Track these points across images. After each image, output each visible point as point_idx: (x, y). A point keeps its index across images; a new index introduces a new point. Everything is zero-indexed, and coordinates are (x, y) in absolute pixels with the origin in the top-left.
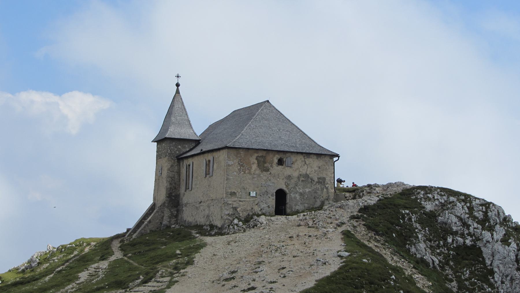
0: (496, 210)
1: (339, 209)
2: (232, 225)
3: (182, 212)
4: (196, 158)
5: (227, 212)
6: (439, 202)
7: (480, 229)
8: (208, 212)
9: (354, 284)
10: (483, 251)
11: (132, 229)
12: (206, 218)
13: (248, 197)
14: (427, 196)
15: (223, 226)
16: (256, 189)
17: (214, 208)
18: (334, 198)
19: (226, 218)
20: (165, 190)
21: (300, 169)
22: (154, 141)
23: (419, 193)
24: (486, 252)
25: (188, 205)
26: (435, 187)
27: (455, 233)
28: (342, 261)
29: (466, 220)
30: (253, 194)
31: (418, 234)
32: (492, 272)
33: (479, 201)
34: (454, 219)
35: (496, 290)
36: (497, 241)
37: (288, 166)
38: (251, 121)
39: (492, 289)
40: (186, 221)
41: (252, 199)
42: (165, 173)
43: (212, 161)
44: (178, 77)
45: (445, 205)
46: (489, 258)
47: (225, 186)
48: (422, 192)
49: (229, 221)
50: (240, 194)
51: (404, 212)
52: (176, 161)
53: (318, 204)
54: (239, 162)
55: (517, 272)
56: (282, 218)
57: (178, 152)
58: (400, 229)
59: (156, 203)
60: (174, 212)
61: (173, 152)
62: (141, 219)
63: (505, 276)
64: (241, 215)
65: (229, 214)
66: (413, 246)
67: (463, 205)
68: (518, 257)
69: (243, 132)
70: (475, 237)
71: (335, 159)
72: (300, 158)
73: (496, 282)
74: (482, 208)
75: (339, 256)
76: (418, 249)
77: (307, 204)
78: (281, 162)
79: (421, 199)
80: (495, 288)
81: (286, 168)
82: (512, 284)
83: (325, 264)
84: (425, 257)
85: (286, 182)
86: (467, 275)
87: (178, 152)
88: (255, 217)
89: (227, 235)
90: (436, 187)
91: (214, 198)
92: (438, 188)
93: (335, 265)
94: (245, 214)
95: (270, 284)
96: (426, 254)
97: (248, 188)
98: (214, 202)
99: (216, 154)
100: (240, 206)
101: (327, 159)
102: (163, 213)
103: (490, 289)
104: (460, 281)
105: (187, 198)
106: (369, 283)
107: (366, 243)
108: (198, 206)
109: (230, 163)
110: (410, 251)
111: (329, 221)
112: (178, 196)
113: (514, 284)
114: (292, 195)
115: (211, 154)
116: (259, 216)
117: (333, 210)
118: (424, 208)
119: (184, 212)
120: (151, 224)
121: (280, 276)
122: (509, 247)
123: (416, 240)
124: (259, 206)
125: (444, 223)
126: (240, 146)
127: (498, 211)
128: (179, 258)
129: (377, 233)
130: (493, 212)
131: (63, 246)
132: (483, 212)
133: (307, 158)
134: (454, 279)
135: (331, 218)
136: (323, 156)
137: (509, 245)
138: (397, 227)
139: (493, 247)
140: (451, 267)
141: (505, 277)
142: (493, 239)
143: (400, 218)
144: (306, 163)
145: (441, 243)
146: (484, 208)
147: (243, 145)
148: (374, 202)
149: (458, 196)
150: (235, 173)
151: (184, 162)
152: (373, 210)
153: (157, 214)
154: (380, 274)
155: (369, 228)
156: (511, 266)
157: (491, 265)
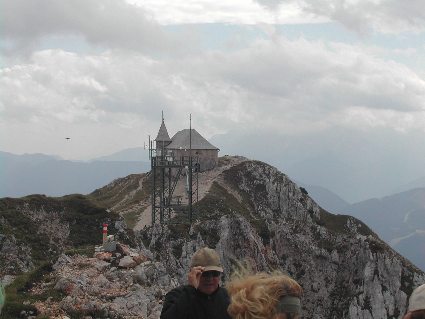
0: (273, 171)
24: (267, 186)
34: (257, 174)
73: (269, 197)
140: (253, 192)
142: (269, 182)
145: (252, 183)
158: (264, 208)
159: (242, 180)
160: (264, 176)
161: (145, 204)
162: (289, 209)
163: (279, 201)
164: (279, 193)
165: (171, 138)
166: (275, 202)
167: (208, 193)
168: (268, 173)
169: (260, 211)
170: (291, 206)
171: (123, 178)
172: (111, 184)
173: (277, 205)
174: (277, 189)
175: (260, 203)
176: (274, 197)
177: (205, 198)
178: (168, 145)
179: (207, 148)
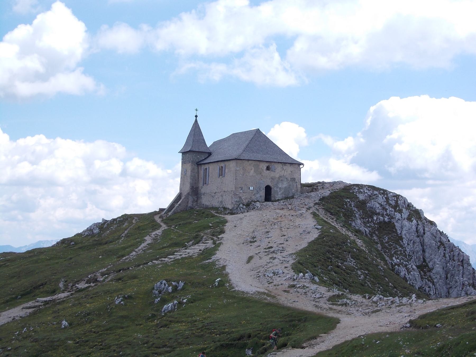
0: (403, 200)
2: (239, 208)
3: (201, 199)
4: (211, 164)
5: (236, 200)
6: (368, 194)
10: (396, 225)
11: (167, 209)
12: (220, 203)
13: (248, 190)
14: (360, 191)
15: (233, 208)
16: (253, 185)
17: (226, 197)
22: (181, 152)
23: (355, 189)
24: (398, 225)
26: (364, 185)
27: (378, 214)
29: (385, 206)
30: (251, 188)
32: (401, 238)
33: (392, 194)
34: (378, 205)
35: (404, 249)
36: (404, 219)
37: (273, 171)
39: (402, 249)
42: (189, 173)
43: (224, 167)
44: (196, 110)
45: (371, 196)
46: (399, 230)
47: (235, 183)
48: (357, 188)
53: (290, 195)
56: (270, 203)
57: (197, 160)
60: (195, 199)
62: (172, 203)
63: (410, 240)
64: (244, 201)
65: (237, 201)
66: (353, 222)
67: (383, 196)
70: (391, 216)
71: (301, 166)
72: (280, 165)
73: (404, 244)
75: (317, 228)
78: (268, 168)
79: (356, 192)
80: (404, 248)
81: (272, 172)
82: (414, 246)
84: (360, 229)
86: (386, 240)
88: (253, 203)
89: (236, 214)
90: (365, 185)
91: (226, 190)
92: (366, 185)
93: (315, 235)
94: (247, 201)
96: (361, 227)
98: (226, 193)
99: (227, 163)
100: (244, 196)
101: (297, 166)
103: (401, 248)
104: (382, 244)
105: (204, 190)
106: (336, 244)
108: (213, 195)
109: (238, 169)
110: (351, 225)
111: (302, 206)
112: (197, 188)
113: (415, 246)
114: (275, 189)
115: (224, 162)
116: (255, 202)
117: (302, 199)
118: (359, 198)
119: (202, 199)
122: (412, 222)
125: (371, 207)
126: (244, 159)
127: (404, 200)
128: (212, 228)
130: (401, 201)
132: (395, 201)
133: (284, 166)
134: (379, 242)
135: (302, 204)
136: (294, 165)
137: (412, 221)
139: (402, 222)
140: (376, 235)
141: (409, 241)
142: (402, 217)
144: (284, 169)
145: (370, 219)
146: (395, 198)
148: (328, 194)
149: (379, 191)
150: (241, 175)
156: (413, 234)
157: (401, 234)
158: (402, 261)
160: (390, 209)
162: (446, 264)
163: (424, 251)
164: (422, 236)
166: (418, 252)
169: (396, 266)
170: (450, 259)
173: (420, 258)
174: (417, 231)
175: (392, 253)
176: (414, 243)
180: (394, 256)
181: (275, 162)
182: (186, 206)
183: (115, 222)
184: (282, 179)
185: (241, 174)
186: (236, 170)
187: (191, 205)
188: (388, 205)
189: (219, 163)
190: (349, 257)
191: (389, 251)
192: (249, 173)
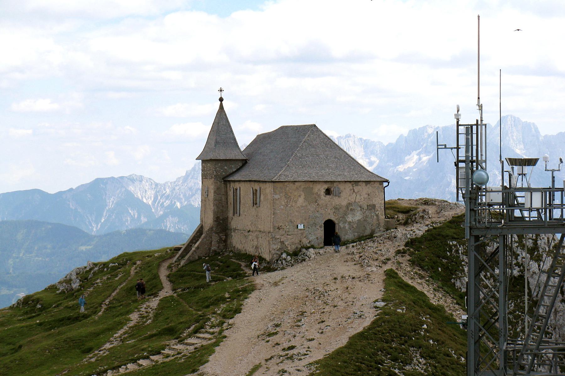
0: (546, 238)
1: (388, 240)
3: (231, 237)
5: (275, 247)
7: (529, 258)
8: (256, 243)
9: (385, 339)
13: (296, 230)
16: (304, 221)
18: (385, 225)
19: (274, 252)
20: (212, 213)
21: (349, 197)
25: (236, 231)
28: (378, 312)
29: (515, 250)
30: (301, 227)
31: (464, 267)
37: (336, 196)
38: (297, 150)
40: (235, 247)
41: (300, 232)
42: (212, 195)
44: (221, 91)
49: (277, 256)
50: (287, 228)
51: (451, 244)
52: (223, 182)
53: (368, 232)
54: (286, 195)
55: (561, 303)
57: (224, 173)
58: (446, 262)
59: (203, 225)
60: (222, 237)
61: (219, 174)
64: (289, 248)
66: (458, 281)
68: (564, 288)
69: (289, 163)
71: (385, 184)
74: (532, 236)
75: (376, 307)
76: (464, 283)
77: (357, 232)
78: (328, 192)
82: (556, 316)
83: (361, 317)
85: (334, 212)
87: (224, 173)
88: (304, 250)
91: (262, 230)
94: (294, 247)
95: (309, 342)
97: (296, 221)
99: (262, 186)
102: (211, 237)
105: (235, 223)
106: (400, 335)
107: (410, 282)
108: (246, 234)
109: (277, 197)
113: (557, 316)
114: (341, 225)
116: (307, 248)
120: (199, 250)
121: (318, 332)
123: (462, 273)
124: (308, 239)
129: (422, 268)
130: (542, 240)
131: (105, 264)
132: (533, 240)
135: (376, 253)
136: (373, 183)
138: (443, 260)
143: (447, 250)
147: (289, 178)
150: (282, 207)
151: (231, 185)
152: (420, 242)
153: (205, 240)
154: (411, 325)
155: (413, 263)
159: (462, 266)
161: (199, 338)
165: (242, 149)
167: (382, 304)
168: (532, 245)
171: (105, 265)
172: (68, 281)
175: (518, 330)
177: (379, 319)
178: (238, 170)
179: (356, 178)
180: (520, 336)
181: (339, 182)
182: (207, 249)
183: (105, 269)
184: (351, 207)
185: (282, 205)
186: (274, 200)
187: (217, 248)
188: (520, 249)
189: (253, 183)
190: (417, 356)
191: (512, 328)
192: (296, 202)
